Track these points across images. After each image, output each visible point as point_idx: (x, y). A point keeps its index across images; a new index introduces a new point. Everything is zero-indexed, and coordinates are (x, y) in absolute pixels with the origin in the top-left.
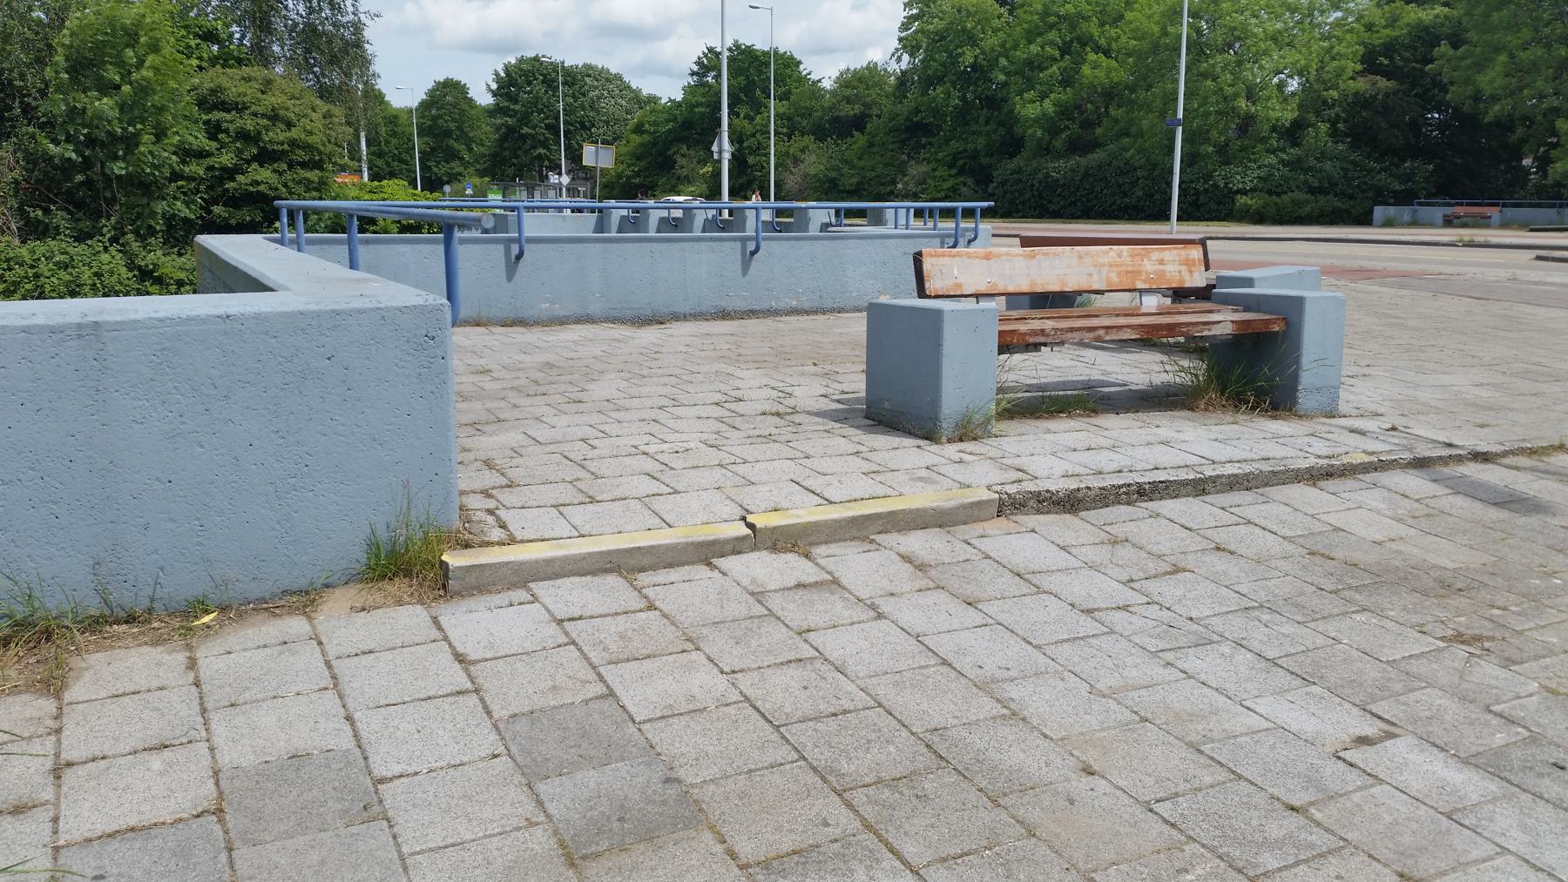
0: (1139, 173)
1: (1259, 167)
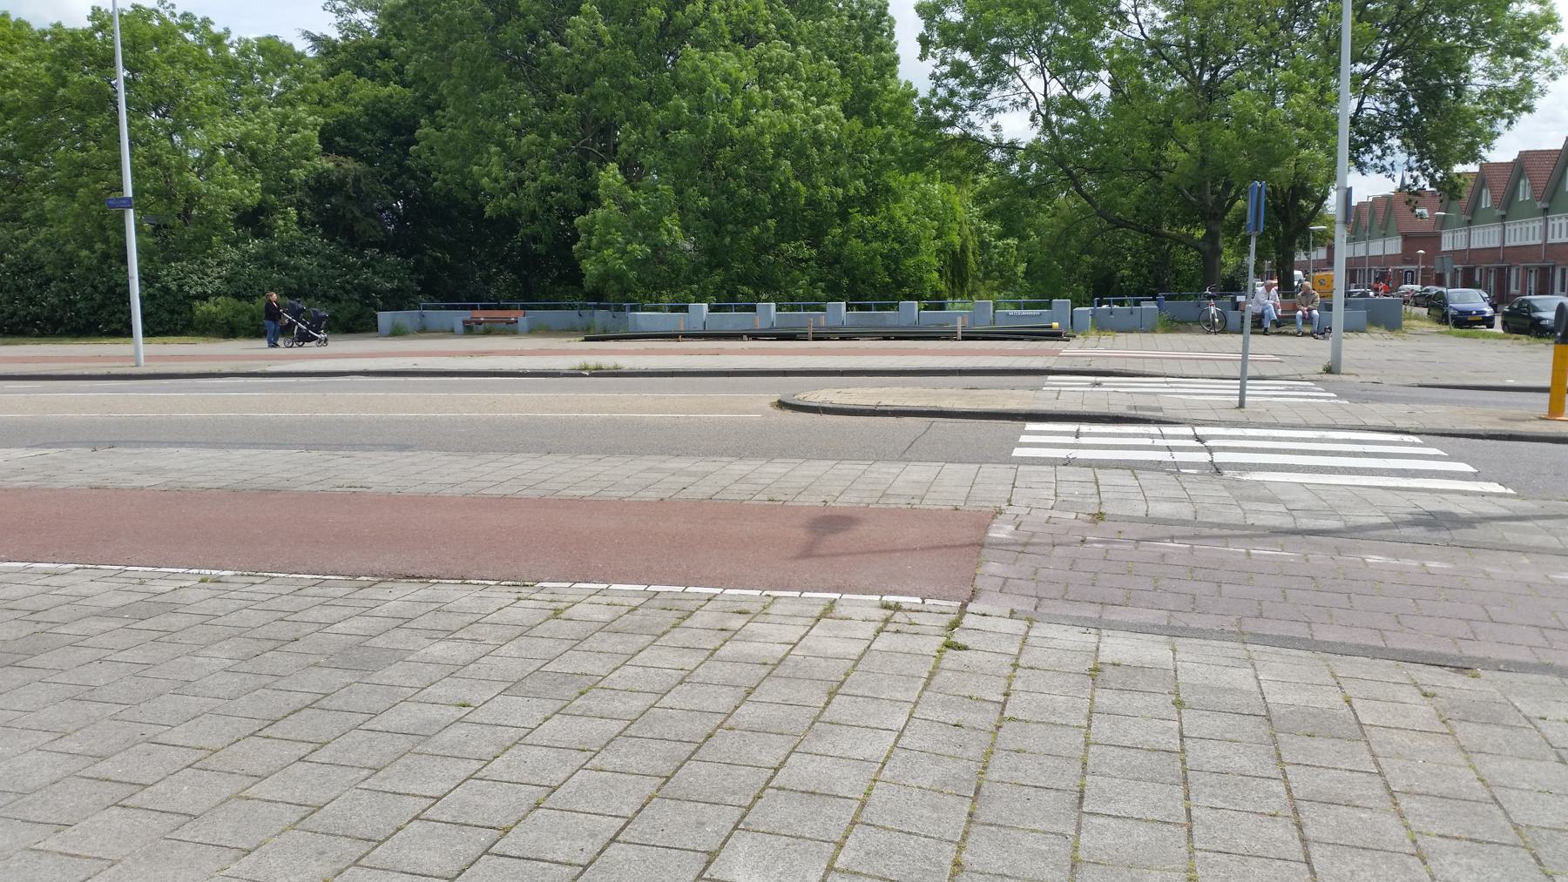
0: (49, 270)
1: (219, 264)
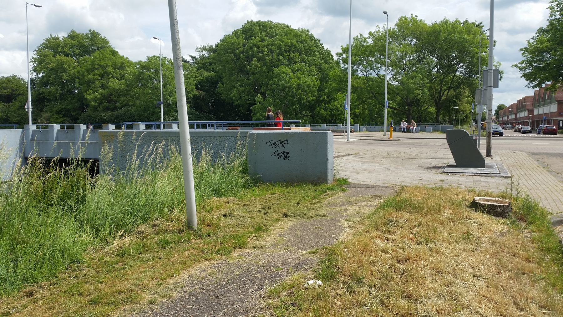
1: (173, 116)
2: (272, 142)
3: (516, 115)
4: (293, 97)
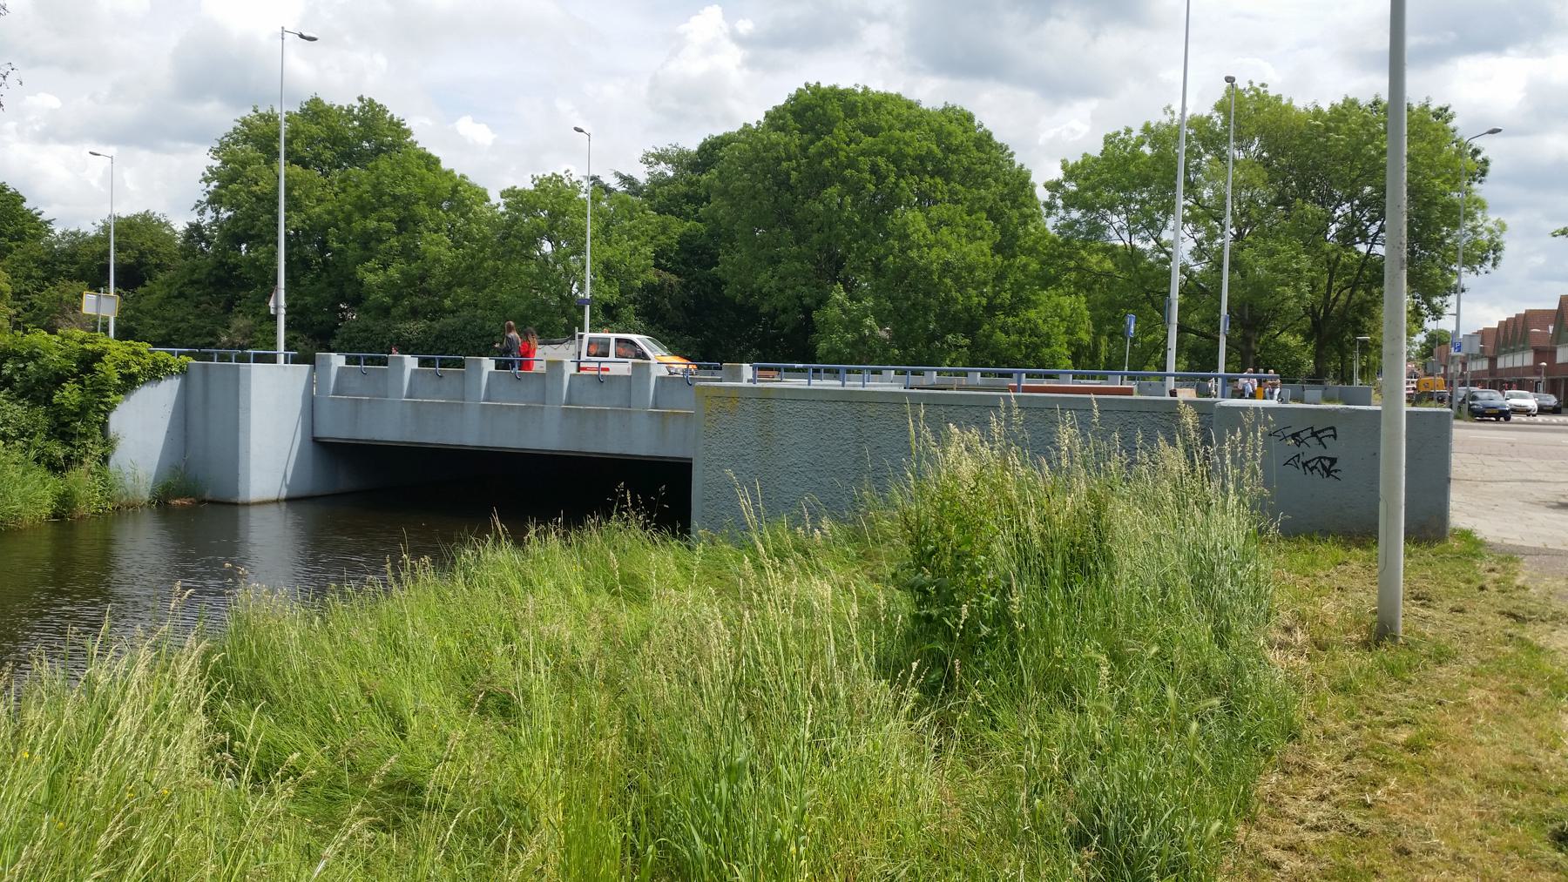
2: (1289, 432)
3: (1493, 360)
4: (927, 294)
